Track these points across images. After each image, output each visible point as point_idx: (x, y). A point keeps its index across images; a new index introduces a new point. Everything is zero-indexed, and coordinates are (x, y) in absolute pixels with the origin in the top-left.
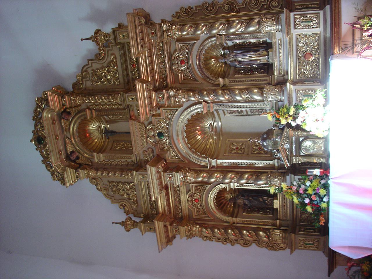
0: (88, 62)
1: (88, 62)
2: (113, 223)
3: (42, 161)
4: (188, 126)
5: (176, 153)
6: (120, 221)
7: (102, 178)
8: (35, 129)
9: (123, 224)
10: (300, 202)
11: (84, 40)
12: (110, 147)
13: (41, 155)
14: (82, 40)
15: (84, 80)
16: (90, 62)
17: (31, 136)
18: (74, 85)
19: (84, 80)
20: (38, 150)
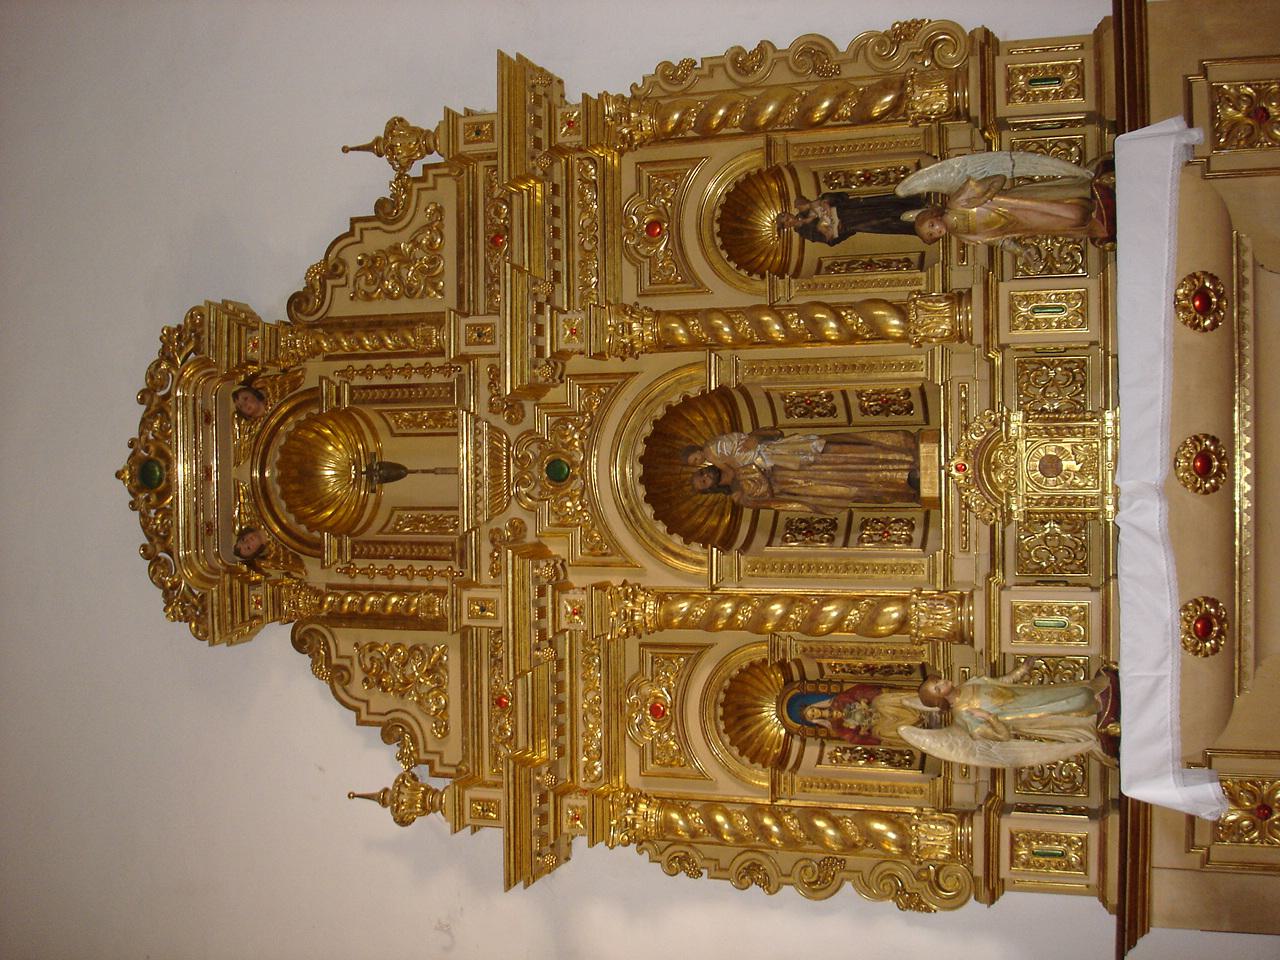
0: (362, 237)
1: (362, 237)
2: (352, 796)
3: (228, 645)
4: (554, 369)
5: (681, 655)
6: (376, 789)
7: (406, 709)
8: (141, 434)
9: (382, 798)
10: (675, 437)
11: (350, 152)
12: (381, 526)
13: (142, 527)
14: (345, 150)
15: (329, 283)
16: (358, 226)
17: (121, 456)
18: (296, 302)
19: (329, 283)
20: (136, 510)
